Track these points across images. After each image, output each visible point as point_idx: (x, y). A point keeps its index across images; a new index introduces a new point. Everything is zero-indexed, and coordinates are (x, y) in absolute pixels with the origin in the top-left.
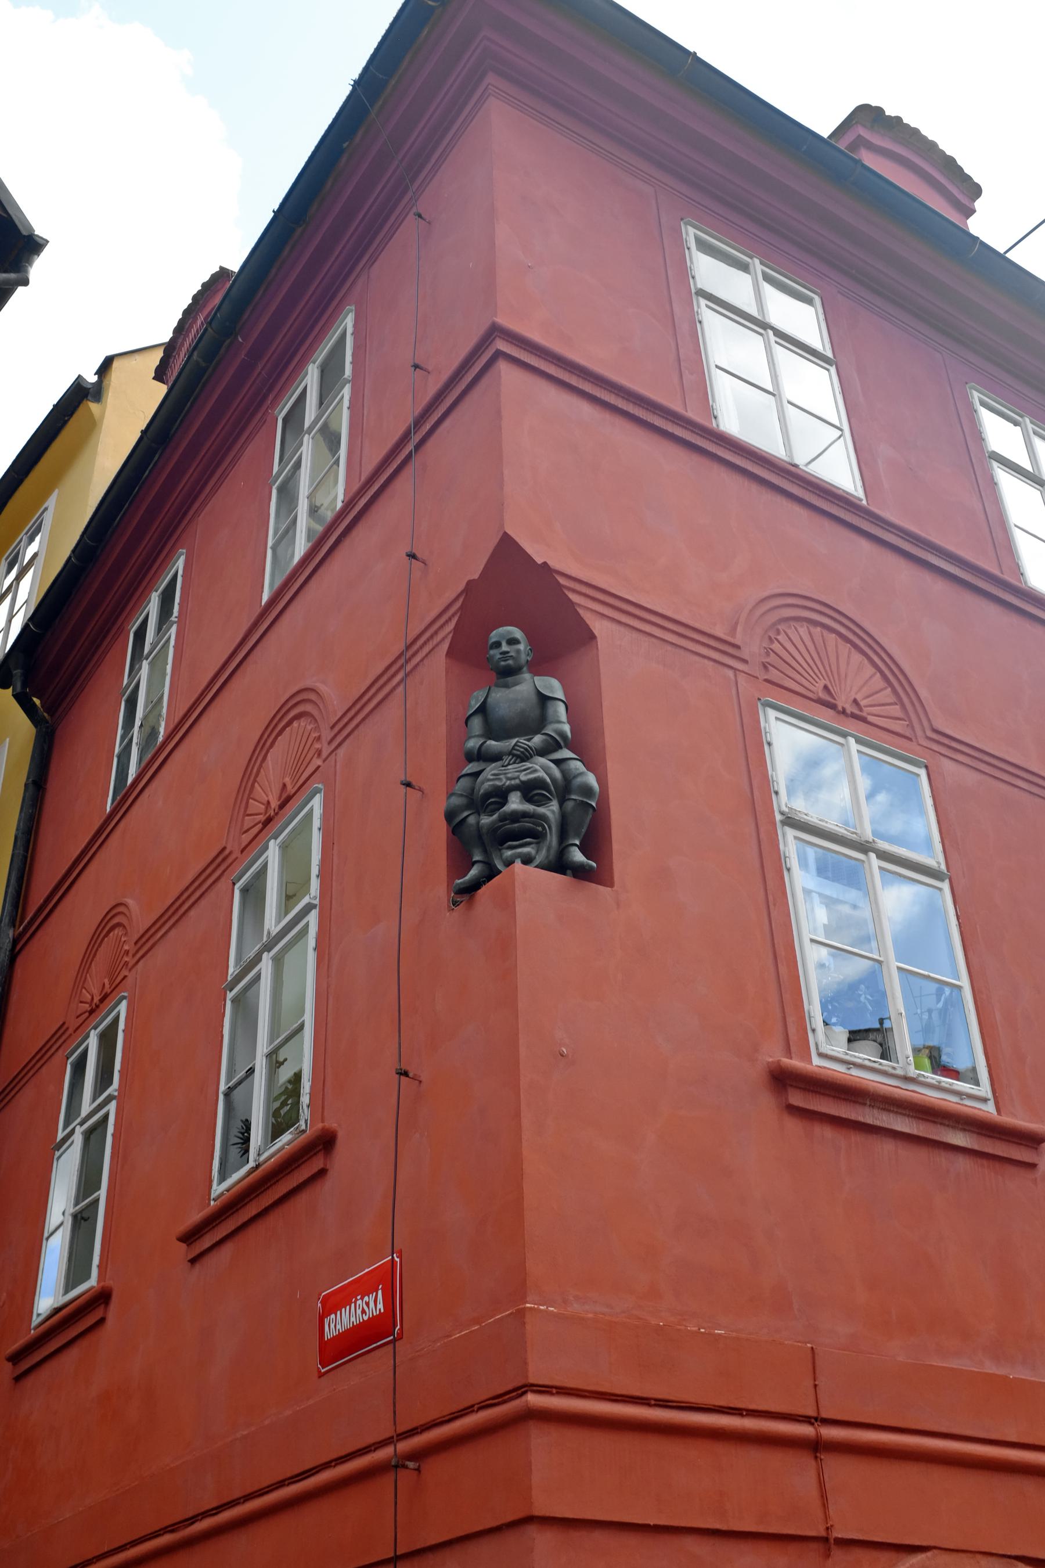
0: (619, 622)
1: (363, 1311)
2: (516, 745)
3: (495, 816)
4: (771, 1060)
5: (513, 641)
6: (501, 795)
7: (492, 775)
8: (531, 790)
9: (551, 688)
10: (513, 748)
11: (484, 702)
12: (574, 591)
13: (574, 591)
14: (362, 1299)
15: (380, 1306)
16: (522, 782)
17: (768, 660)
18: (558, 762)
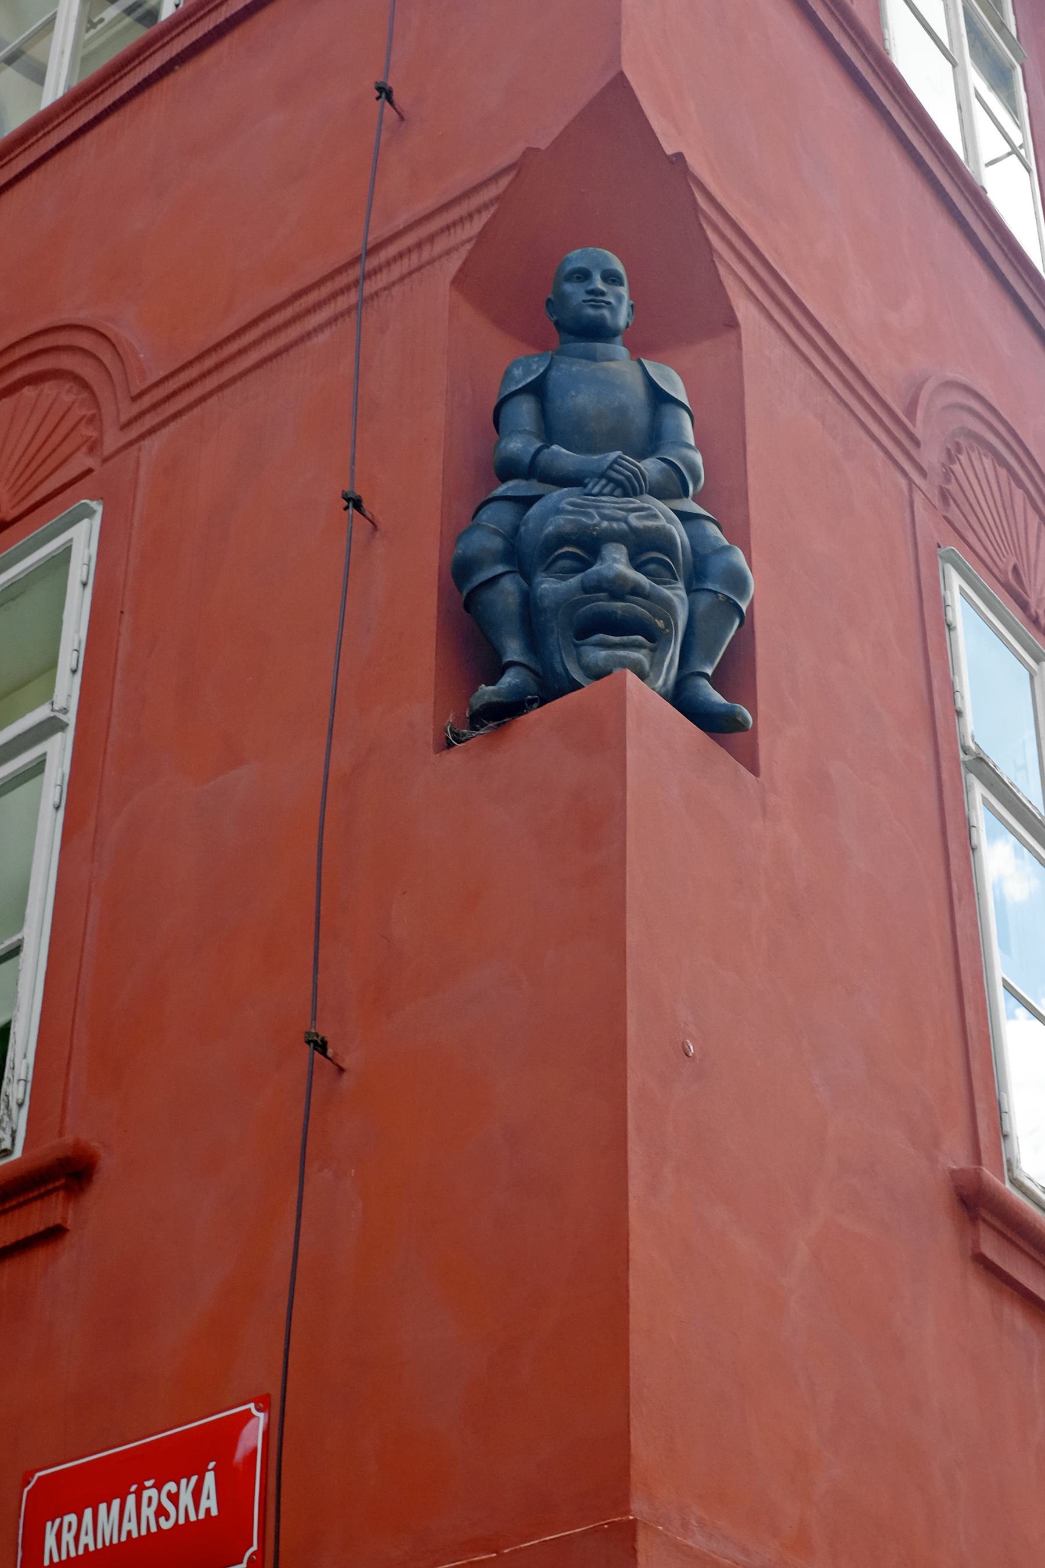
0: (770, 318)
1: (161, 1512)
2: (615, 462)
3: (575, 580)
4: (955, 1167)
5: (611, 278)
6: (589, 546)
7: (558, 510)
8: (647, 547)
9: (671, 382)
10: (610, 467)
11: (544, 376)
12: (716, 228)
13: (716, 228)
14: (159, 1487)
15: (210, 1503)
16: (633, 530)
17: (948, 487)
18: (685, 517)
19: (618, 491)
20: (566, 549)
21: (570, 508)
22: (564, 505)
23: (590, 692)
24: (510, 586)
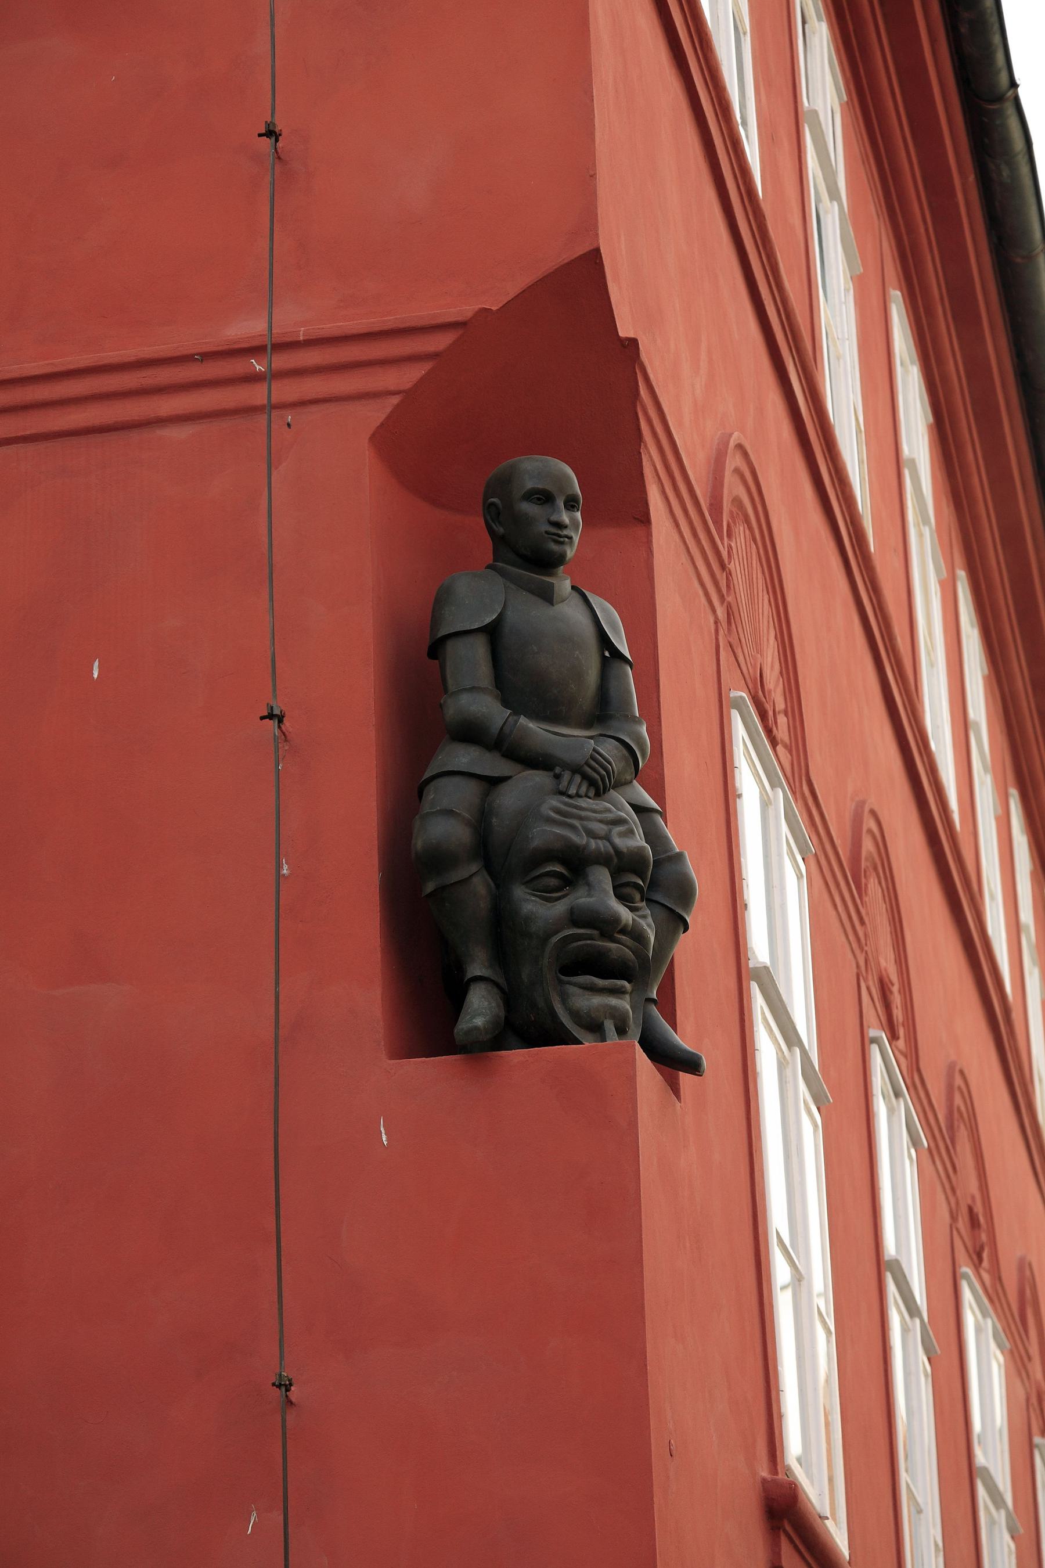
11: (500, 618)
19: (592, 793)
20: (550, 868)
21: (553, 814)
22: (546, 810)
23: (586, 1049)
24: (481, 886)
